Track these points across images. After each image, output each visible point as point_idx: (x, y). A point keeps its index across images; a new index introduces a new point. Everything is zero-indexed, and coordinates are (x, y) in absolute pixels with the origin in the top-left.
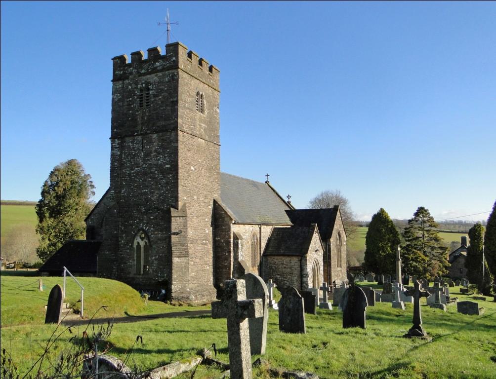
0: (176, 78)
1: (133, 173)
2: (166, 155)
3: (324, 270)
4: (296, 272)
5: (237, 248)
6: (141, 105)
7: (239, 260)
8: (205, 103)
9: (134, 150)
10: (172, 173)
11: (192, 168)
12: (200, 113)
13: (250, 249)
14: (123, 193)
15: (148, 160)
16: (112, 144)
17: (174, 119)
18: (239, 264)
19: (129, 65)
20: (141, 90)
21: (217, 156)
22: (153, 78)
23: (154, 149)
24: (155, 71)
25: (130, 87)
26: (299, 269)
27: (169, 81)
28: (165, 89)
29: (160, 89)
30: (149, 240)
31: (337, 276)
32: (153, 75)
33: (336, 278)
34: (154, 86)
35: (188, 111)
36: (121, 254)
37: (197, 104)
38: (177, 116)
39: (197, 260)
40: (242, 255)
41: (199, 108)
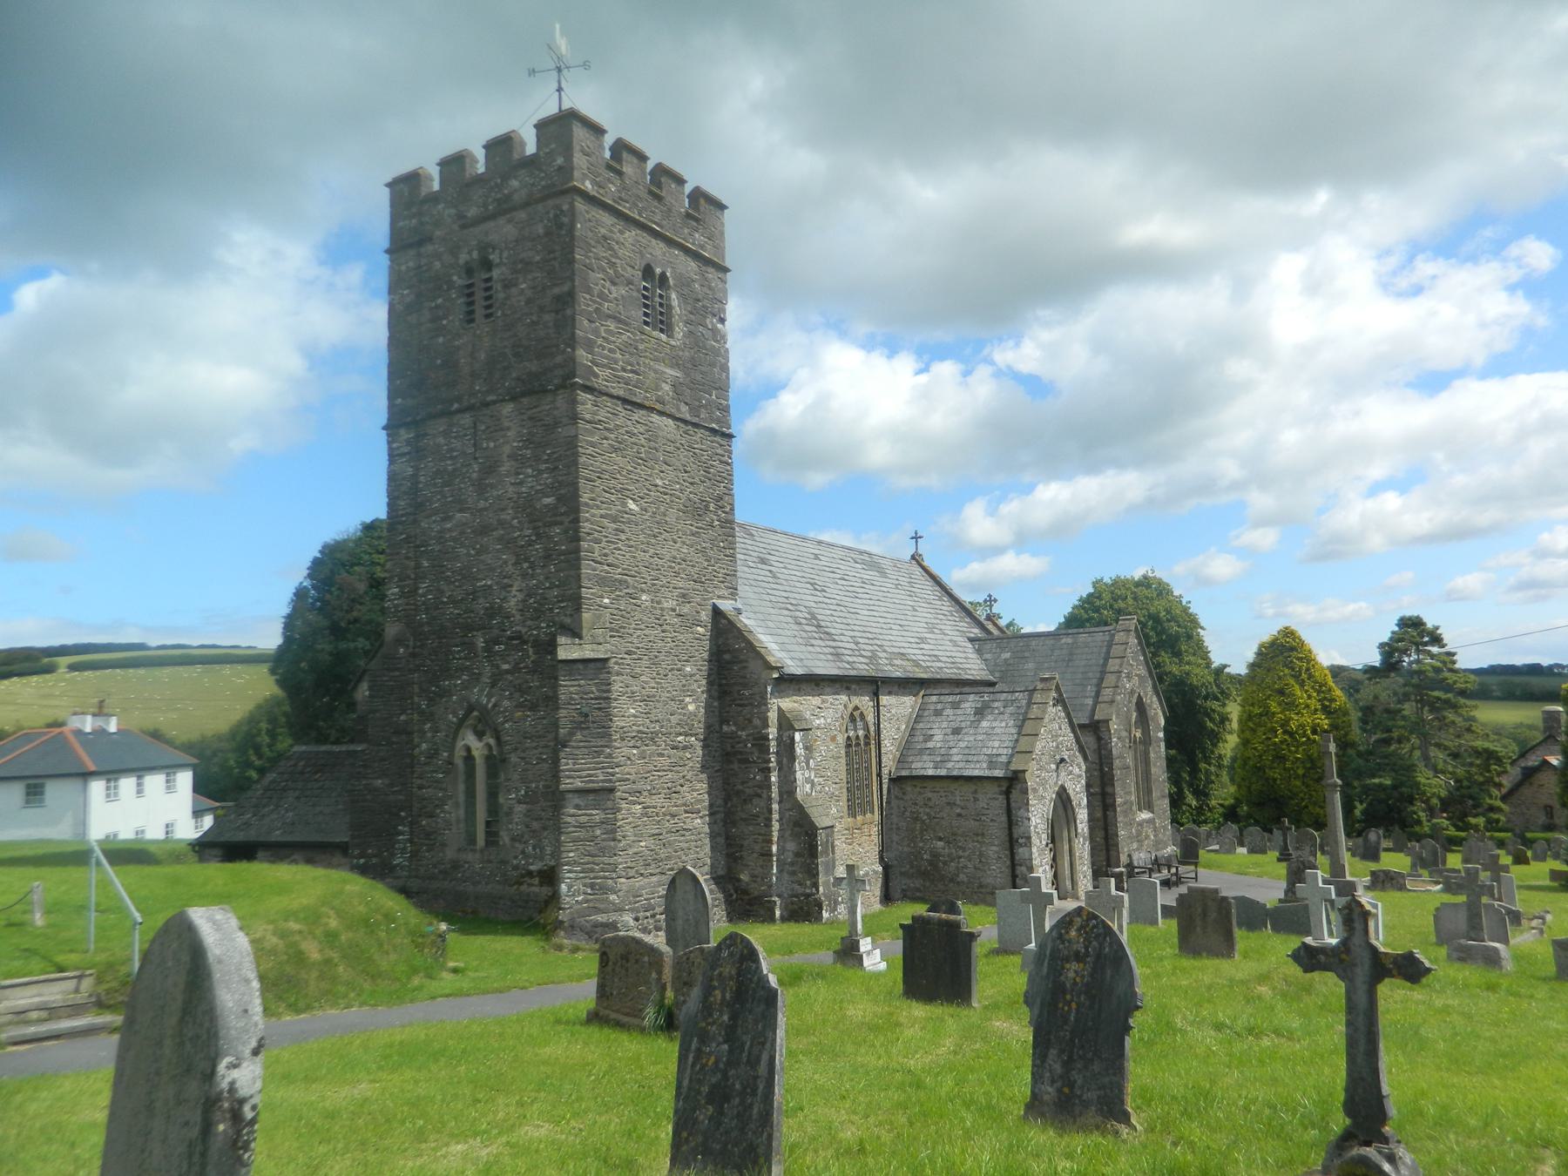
0: (565, 220)
1: (450, 530)
2: (543, 467)
3: (1091, 819)
4: (997, 830)
5: (792, 757)
6: (470, 317)
7: (799, 794)
8: (675, 303)
9: (452, 458)
10: (561, 523)
11: (632, 506)
12: (656, 333)
13: (843, 761)
14: (423, 595)
15: (492, 486)
16: (389, 443)
17: (564, 351)
18: (800, 809)
19: (434, 198)
20: (469, 271)
21: (721, 467)
22: (502, 231)
23: (507, 450)
24: (505, 207)
25: (437, 264)
26: (1004, 818)
27: (548, 234)
28: (538, 258)
29: (521, 261)
30: (498, 739)
31: (1138, 838)
32: (501, 221)
33: (1135, 845)
34: (505, 254)
35: (612, 326)
36: (420, 788)
37: (646, 306)
38: (572, 342)
39: (658, 800)
40: (808, 780)
41: (655, 317)
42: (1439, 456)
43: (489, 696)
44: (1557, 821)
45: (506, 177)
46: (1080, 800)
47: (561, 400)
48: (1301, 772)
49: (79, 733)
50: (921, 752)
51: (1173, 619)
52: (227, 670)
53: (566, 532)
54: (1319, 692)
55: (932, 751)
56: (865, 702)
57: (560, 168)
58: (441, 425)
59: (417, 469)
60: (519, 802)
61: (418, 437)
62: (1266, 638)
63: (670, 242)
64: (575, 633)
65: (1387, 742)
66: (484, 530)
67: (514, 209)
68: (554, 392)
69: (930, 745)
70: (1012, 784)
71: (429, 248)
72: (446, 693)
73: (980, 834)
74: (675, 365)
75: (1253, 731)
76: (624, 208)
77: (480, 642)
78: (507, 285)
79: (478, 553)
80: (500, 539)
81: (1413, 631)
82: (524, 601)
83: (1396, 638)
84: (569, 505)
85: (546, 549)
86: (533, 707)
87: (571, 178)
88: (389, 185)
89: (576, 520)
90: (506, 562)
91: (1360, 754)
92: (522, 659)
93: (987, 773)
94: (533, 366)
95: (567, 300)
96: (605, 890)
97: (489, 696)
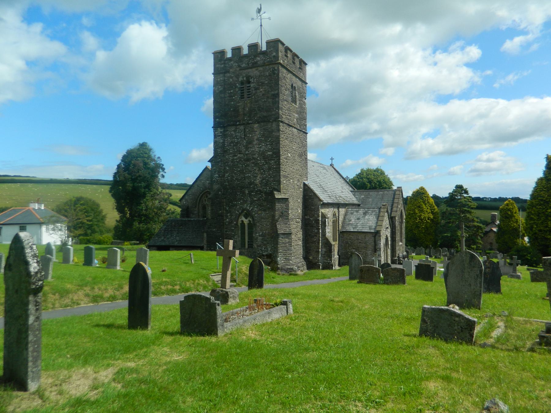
1: (236, 159)
6: (242, 97)
19: (230, 59)
22: (254, 72)
23: (256, 137)
24: (255, 65)
25: (231, 80)
26: (373, 243)
27: (270, 75)
32: (254, 69)
35: (286, 103)
36: (226, 231)
38: (278, 108)
42: (446, 126)
43: (250, 207)
44: (493, 247)
45: (255, 56)
46: (389, 239)
47: (274, 125)
48: (423, 231)
49: (34, 209)
50: (349, 224)
51: (385, 183)
52: (30, 185)
53: (276, 162)
54: (430, 207)
55: (352, 224)
56: (336, 210)
57: (274, 56)
58: (233, 128)
59: (224, 140)
60: (260, 236)
61: (224, 131)
62: (415, 190)
63: (297, 77)
64: (279, 191)
65: (449, 223)
66: (248, 160)
67: (259, 66)
68: (272, 122)
69: (351, 222)
70: (377, 234)
71: (228, 75)
72: (236, 205)
73: (366, 248)
74: (297, 114)
75: (410, 218)
76: (288, 67)
77: (247, 192)
78: (256, 89)
79: (246, 166)
80: (253, 163)
81: (460, 189)
82: (261, 181)
83: (454, 191)
84: (277, 155)
85: (269, 167)
86: (265, 210)
87: (278, 60)
88: (213, 53)
89: (280, 159)
90: (255, 169)
91: (441, 226)
92: (261, 197)
93: (369, 231)
94: (265, 114)
95: (277, 95)
96: (289, 260)
97: (250, 207)
